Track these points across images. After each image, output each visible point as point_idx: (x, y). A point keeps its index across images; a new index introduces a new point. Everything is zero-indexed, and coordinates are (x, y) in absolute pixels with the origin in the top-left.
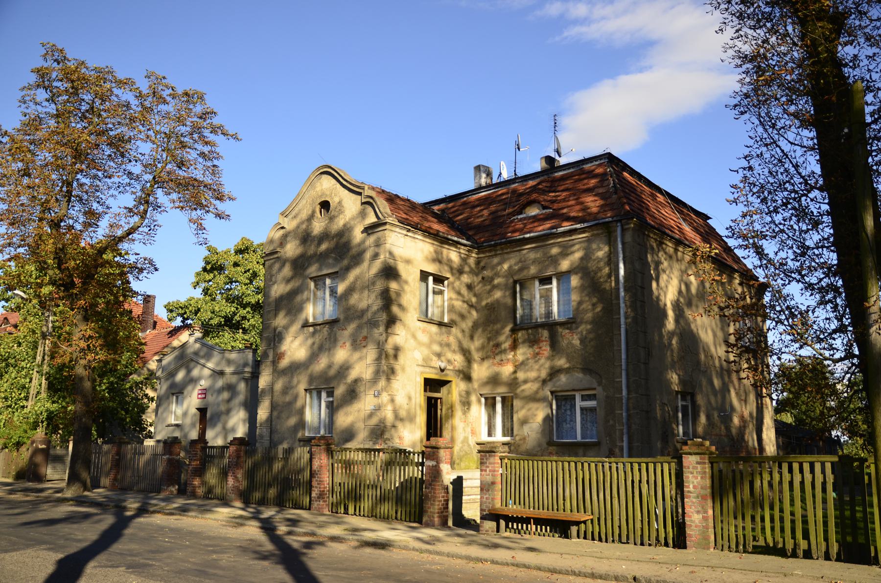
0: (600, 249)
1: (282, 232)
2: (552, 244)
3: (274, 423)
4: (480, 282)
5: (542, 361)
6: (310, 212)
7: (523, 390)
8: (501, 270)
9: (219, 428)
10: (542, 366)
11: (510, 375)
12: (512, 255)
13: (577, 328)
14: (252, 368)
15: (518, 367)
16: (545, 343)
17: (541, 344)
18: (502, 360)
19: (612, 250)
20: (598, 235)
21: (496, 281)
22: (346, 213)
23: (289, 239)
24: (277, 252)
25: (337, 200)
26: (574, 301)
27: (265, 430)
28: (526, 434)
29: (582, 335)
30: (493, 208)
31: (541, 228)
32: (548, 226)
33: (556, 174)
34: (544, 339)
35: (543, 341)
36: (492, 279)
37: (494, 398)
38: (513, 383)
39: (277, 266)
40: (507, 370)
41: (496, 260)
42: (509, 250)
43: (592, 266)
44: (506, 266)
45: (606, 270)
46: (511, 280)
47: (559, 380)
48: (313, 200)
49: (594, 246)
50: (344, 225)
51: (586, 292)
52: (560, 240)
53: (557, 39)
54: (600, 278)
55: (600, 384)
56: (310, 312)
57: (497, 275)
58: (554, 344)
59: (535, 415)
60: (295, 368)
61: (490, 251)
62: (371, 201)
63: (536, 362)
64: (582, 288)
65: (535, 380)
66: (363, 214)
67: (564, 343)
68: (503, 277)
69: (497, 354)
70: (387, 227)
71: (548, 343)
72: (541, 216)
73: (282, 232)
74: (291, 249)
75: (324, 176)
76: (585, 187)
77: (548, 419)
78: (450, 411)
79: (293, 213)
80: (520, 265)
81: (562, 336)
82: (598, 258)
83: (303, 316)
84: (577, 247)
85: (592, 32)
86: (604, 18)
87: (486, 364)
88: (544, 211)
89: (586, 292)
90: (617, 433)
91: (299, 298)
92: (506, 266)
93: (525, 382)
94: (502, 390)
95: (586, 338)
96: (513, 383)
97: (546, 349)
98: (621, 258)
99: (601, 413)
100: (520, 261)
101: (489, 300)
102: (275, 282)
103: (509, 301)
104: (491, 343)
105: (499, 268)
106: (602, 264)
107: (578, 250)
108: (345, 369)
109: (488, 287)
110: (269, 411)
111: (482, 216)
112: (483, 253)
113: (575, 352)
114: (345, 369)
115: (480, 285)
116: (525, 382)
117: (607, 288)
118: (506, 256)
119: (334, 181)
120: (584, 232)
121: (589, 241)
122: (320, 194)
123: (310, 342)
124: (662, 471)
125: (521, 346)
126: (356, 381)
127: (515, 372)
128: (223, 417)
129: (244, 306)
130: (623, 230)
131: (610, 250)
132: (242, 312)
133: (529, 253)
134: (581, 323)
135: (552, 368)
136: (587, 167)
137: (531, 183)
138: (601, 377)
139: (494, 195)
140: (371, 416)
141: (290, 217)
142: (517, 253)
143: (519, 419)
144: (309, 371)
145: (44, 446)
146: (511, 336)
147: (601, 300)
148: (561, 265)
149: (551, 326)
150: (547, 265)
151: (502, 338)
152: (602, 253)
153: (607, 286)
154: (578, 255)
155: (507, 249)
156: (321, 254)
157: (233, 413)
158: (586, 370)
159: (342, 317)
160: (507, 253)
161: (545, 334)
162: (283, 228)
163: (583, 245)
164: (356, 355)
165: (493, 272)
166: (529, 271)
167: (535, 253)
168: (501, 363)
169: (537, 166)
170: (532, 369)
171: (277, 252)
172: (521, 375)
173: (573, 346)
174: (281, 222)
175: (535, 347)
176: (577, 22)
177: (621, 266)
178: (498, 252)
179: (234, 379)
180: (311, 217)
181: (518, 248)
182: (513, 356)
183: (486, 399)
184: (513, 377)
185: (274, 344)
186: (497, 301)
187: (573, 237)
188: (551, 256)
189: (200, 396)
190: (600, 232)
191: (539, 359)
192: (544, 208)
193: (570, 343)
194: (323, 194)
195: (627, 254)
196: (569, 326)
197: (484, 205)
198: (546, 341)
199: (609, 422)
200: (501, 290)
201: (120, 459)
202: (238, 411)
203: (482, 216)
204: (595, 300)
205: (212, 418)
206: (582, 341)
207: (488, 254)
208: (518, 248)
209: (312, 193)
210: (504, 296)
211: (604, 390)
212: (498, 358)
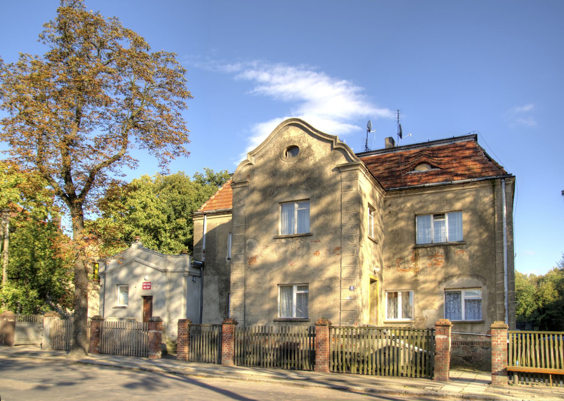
0: (486, 196)
1: (248, 167)
2: (447, 191)
3: (247, 308)
4: (387, 215)
5: (439, 268)
6: (278, 153)
7: (422, 288)
8: (404, 207)
9: (165, 309)
10: (438, 272)
11: (412, 278)
12: (414, 197)
13: (467, 248)
14: (189, 269)
15: (417, 273)
16: (440, 257)
17: (438, 258)
18: (405, 268)
19: (496, 197)
20: (485, 187)
21: (400, 215)
22: (315, 155)
23: (256, 173)
24: (246, 182)
25: (305, 145)
26: (465, 230)
27: (238, 313)
28: (424, 316)
29: (471, 252)
30: (387, 165)
31: (436, 180)
32: (440, 179)
33: (433, 146)
34: (440, 254)
35: (439, 256)
36: (397, 213)
37: (396, 294)
38: (415, 283)
39: (245, 192)
40: (410, 274)
41: (400, 200)
42: (411, 194)
43: (480, 207)
44: (409, 205)
45: (491, 210)
46: (413, 215)
47: (452, 282)
48: (280, 144)
49: (481, 194)
50: (314, 165)
51: (474, 225)
52: (453, 189)
53: (251, 92)
54: (486, 216)
55: (484, 284)
56: (280, 227)
57: (401, 210)
58: (448, 257)
59: (433, 304)
60: (267, 267)
61: (396, 194)
62: (343, 147)
63: (433, 270)
64: (472, 222)
65: (432, 281)
66: (333, 158)
67: (456, 258)
68: (406, 212)
69: (401, 264)
70: (359, 167)
71: (444, 257)
72: (432, 173)
73: (248, 167)
74: (258, 180)
75: (291, 128)
76: (462, 155)
77: (441, 307)
78: (375, 301)
79: (261, 154)
80: (420, 205)
81: (455, 253)
82: (484, 202)
83: (273, 230)
84: (467, 194)
85: (271, 90)
86: (278, 83)
87: (392, 270)
88: (433, 170)
89: (474, 225)
90: (498, 315)
91: (269, 217)
92: (409, 205)
93: (425, 282)
94: (405, 287)
95: (474, 255)
96: (415, 283)
97: (441, 260)
98: (505, 203)
99: (484, 304)
100: (421, 202)
101: (394, 228)
102: (243, 205)
103: (411, 228)
104: (396, 257)
105: (403, 206)
106: (487, 207)
107: (468, 196)
108: (320, 269)
109: (394, 219)
110: (243, 299)
111: (379, 170)
112: (390, 195)
113: (465, 264)
114: (320, 269)
115: (387, 217)
116: (425, 282)
117: (491, 223)
118: (409, 198)
119: (301, 131)
120: (474, 184)
121: (477, 190)
122: (287, 140)
123: (283, 249)
124: (544, 341)
125: (421, 258)
126: (332, 279)
127: (416, 276)
128: (167, 303)
129: (138, 226)
130: (506, 184)
131: (494, 197)
132: (137, 231)
133: (428, 196)
134: (470, 245)
135: (446, 274)
136: (458, 142)
137: (413, 151)
138: (485, 280)
139: (383, 157)
140: (348, 303)
141: (257, 156)
142: (419, 196)
143: (419, 307)
144: (284, 269)
145: (12, 320)
146: (413, 252)
147: (487, 230)
148: (454, 206)
149: (446, 246)
150: (444, 205)
151: (406, 253)
152: (487, 199)
153: (491, 222)
154: (469, 200)
155: (410, 193)
156: (291, 185)
157: (175, 299)
158: (475, 274)
159: (315, 233)
160: (409, 196)
161: (441, 251)
162: (250, 164)
163: (475, 192)
164: (332, 259)
165: (398, 208)
166: (428, 209)
167: (433, 197)
168: (404, 270)
169: (382, 145)
170: (430, 274)
171: (246, 182)
172: (421, 278)
173: (463, 260)
174: (249, 159)
175: (433, 259)
176: (262, 84)
177: (505, 207)
178: (403, 195)
179: (174, 276)
180: (279, 157)
181: (420, 193)
182: (414, 265)
183: (389, 293)
184: (414, 279)
185: (245, 251)
186: (401, 229)
187: (465, 187)
188: (446, 200)
189: (145, 287)
190: (487, 185)
191: (436, 268)
192: (433, 167)
193: (461, 258)
194: (290, 141)
195: (508, 201)
196: (461, 246)
197: (377, 163)
198: (442, 256)
199: (491, 309)
200: (405, 221)
201: (99, 331)
202: (180, 299)
203: (379, 170)
204: (481, 230)
205: (157, 303)
206: (471, 257)
207: (393, 196)
208: (420, 193)
209: (280, 139)
210: (408, 225)
211: (488, 288)
212: (402, 267)
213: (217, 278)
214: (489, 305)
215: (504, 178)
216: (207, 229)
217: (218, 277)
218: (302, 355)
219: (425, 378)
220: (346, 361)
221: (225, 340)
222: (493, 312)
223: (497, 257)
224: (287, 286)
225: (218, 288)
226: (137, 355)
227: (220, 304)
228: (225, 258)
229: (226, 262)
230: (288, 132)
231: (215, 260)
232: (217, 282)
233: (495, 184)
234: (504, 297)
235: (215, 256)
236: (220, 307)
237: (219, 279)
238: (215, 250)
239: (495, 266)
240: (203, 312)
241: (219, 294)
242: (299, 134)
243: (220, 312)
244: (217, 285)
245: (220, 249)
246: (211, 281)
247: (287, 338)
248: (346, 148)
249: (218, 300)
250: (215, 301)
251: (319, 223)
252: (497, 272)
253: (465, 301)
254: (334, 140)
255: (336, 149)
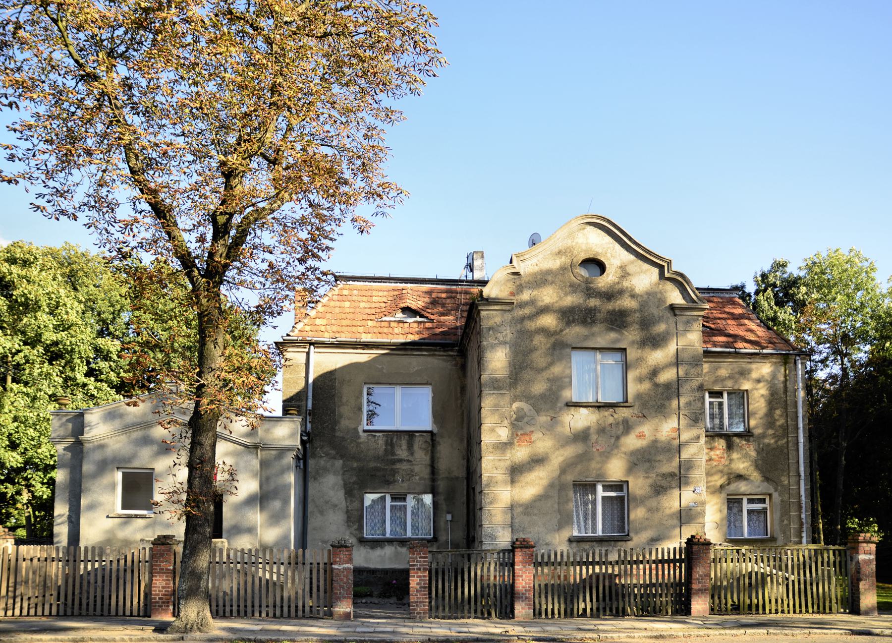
62: (680, 279)
119: (608, 239)
190: (778, 360)
211: (779, 495)
213: (339, 463)
214: (782, 516)
215: (799, 355)
216: (314, 372)
217: (341, 461)
218: (117, 602)
219: (849, 613)
220: (444, 607)
221: (522, 576)
222: (787, 525)
223: (790, 456)
224: (580, 485)
225: (342, 482)
226: (278, 613)
227: (347, 512)
228: (356, 429)
229: (359, 437)
230: (584, 235)
231: (334, 430)
232: (341, 473)
233: (788, 361)
234: (801, 507)
235: (336, 422)
236: (348, 517)
237: (344, 466)
238: (334, 412)
239: (789, 465)
240: (310, 527)
241: (346, 493)
242: (604, 242)
243: (349, 526)
244: (340, 478)
245: (345, 410)
246: (326, 470)
247: (724, 565)
248: (685, 281)
249: (344, 504)
250: (336, 506)
251: (643, 388)
252: (791, 474)
253: (748, 511)
254: (665, 265)
255: (669, 279)
